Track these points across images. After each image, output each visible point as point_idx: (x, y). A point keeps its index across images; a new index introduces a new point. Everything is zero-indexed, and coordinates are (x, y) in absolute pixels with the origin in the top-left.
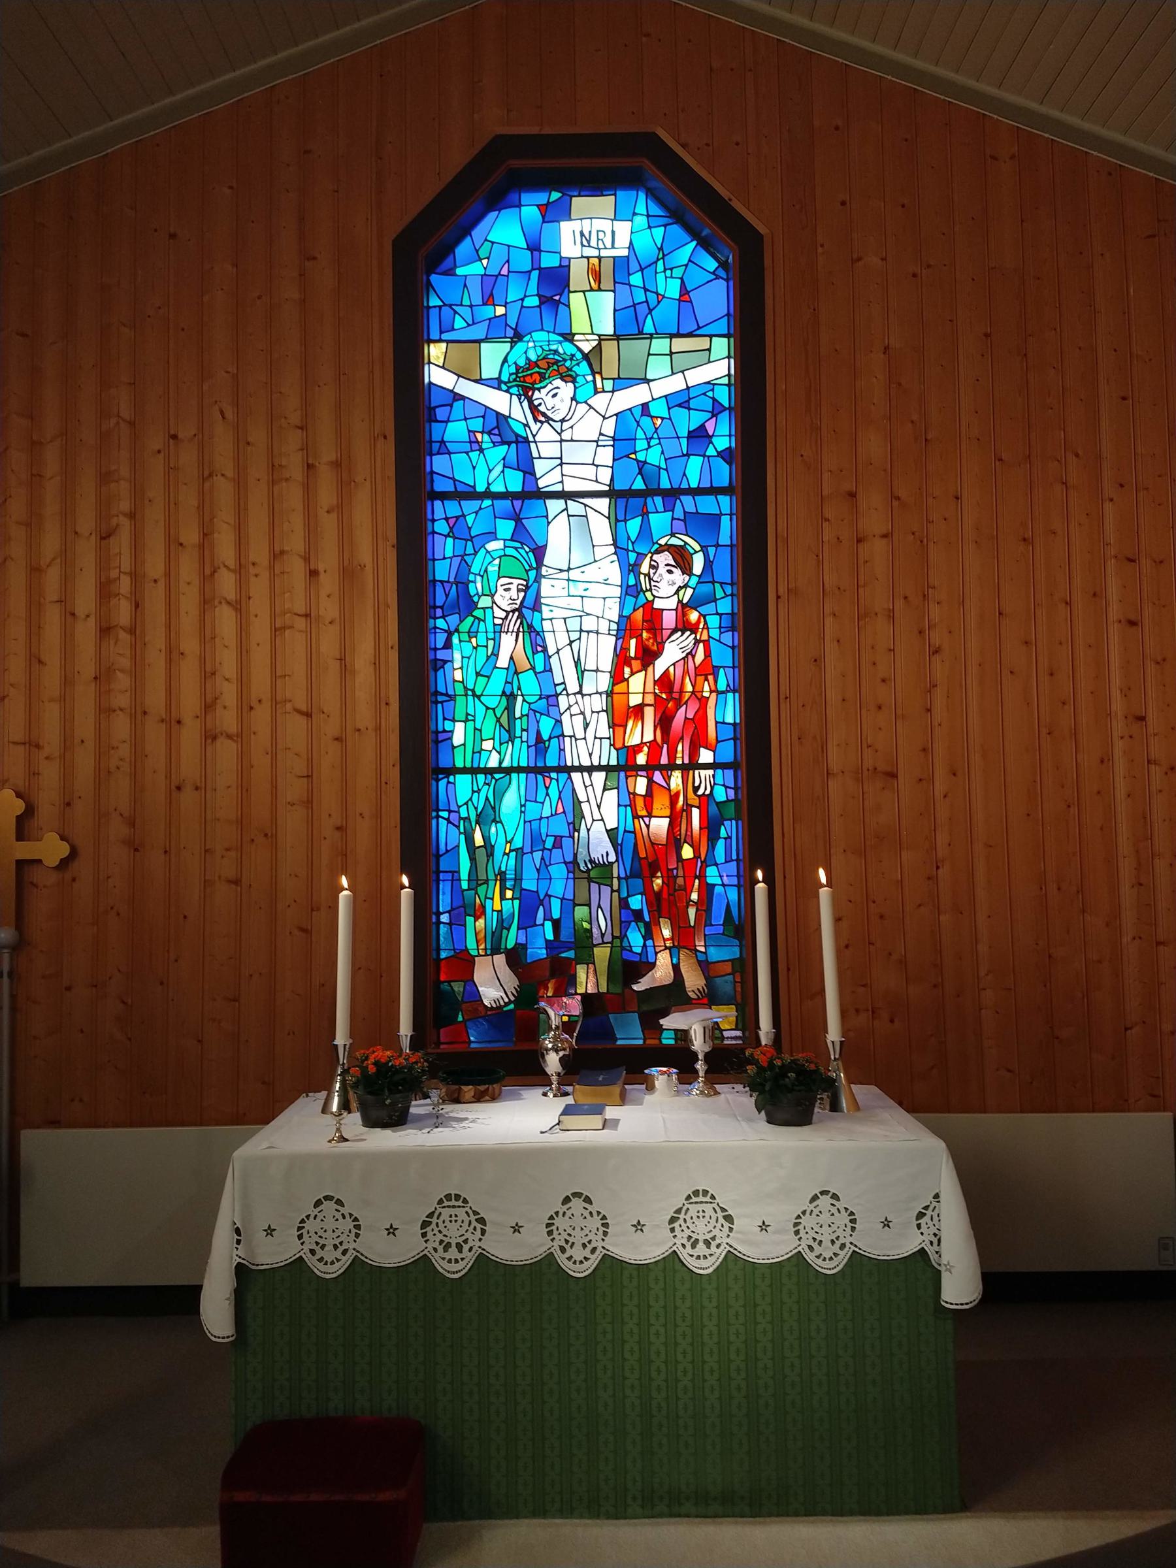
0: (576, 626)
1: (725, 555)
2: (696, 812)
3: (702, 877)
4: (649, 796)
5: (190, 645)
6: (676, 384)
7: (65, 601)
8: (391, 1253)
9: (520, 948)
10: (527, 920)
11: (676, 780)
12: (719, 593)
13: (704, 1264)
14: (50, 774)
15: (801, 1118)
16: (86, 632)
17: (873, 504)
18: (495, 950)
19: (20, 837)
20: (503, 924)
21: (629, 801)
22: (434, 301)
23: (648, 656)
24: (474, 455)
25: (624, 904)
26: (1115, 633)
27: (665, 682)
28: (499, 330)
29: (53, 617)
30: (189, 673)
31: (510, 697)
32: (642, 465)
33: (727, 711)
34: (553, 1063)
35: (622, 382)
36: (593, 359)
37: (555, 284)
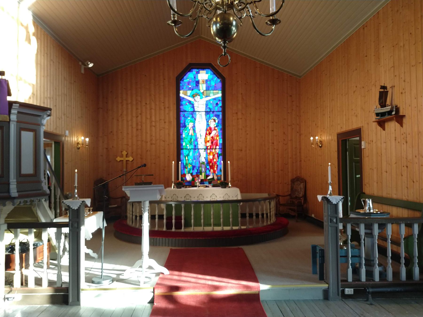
0: (201, 129)
4: (210, 153)
5: (148, 131)
7: (132, 126)
10: (193, 169)
11: (213, 151)
14: (130, 149)
16: (135, 130)
17: (240, 114)
18: (189, 173)
19: (126, 157)
20: (190, 170)
21: (207, 153)
22: (181, 85)
23: (210, 134)
25: (206, 167)
26: (270, 132)
27: (212, 137)
28: (190, 89)
29: (130, 128)
30: (148, 135)
31: (191, 139)
33: (220, 141)
35: (206, 96)
37: (198, 83)
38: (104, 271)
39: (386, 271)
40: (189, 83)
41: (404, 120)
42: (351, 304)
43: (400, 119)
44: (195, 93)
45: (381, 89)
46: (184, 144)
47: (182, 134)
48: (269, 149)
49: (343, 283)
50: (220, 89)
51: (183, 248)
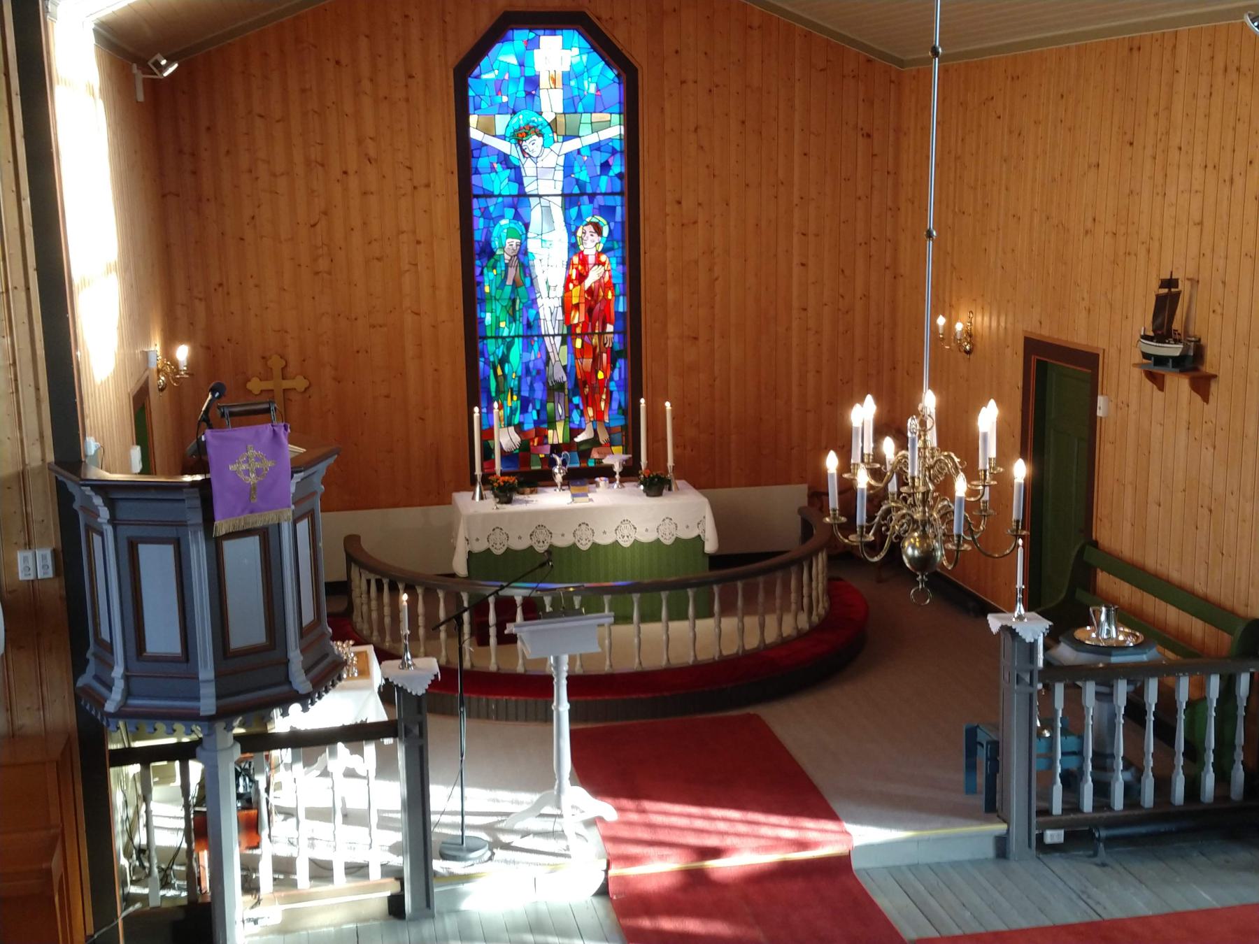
1: (619, 227)
2: (605, 355)
3: (607, 387)
6: (593, 139)
8: (519, 545)
9: (521, 424)
10: (524, 410)
11: (595, 340)
12: (616, 246)
13: (626, 543)
15: (659, 494)
18: (509, 425)
20: (513, 412)
21: (573, 351)
22: (471, 93)
23: (582, 277)
24: (493, 175)
27: (590, 291)
31: (514, 301)
32: (577, 180)
34: (559, 478)
35: (567, 138)
36: (553, 125)
37: (533, 84)
38: (466, 818)
39: (1139, 780)
40: (499, 87)
41: (1214, 387)
42: (1058, 864)
43: (1202, 385)
44: (522, 124)
45: (1161, 287)
46: (488, 318)
47: (481, 284)
48: (788, 329)
49: (1041, 819)
50: (616, 108)
51: (590, 725)
